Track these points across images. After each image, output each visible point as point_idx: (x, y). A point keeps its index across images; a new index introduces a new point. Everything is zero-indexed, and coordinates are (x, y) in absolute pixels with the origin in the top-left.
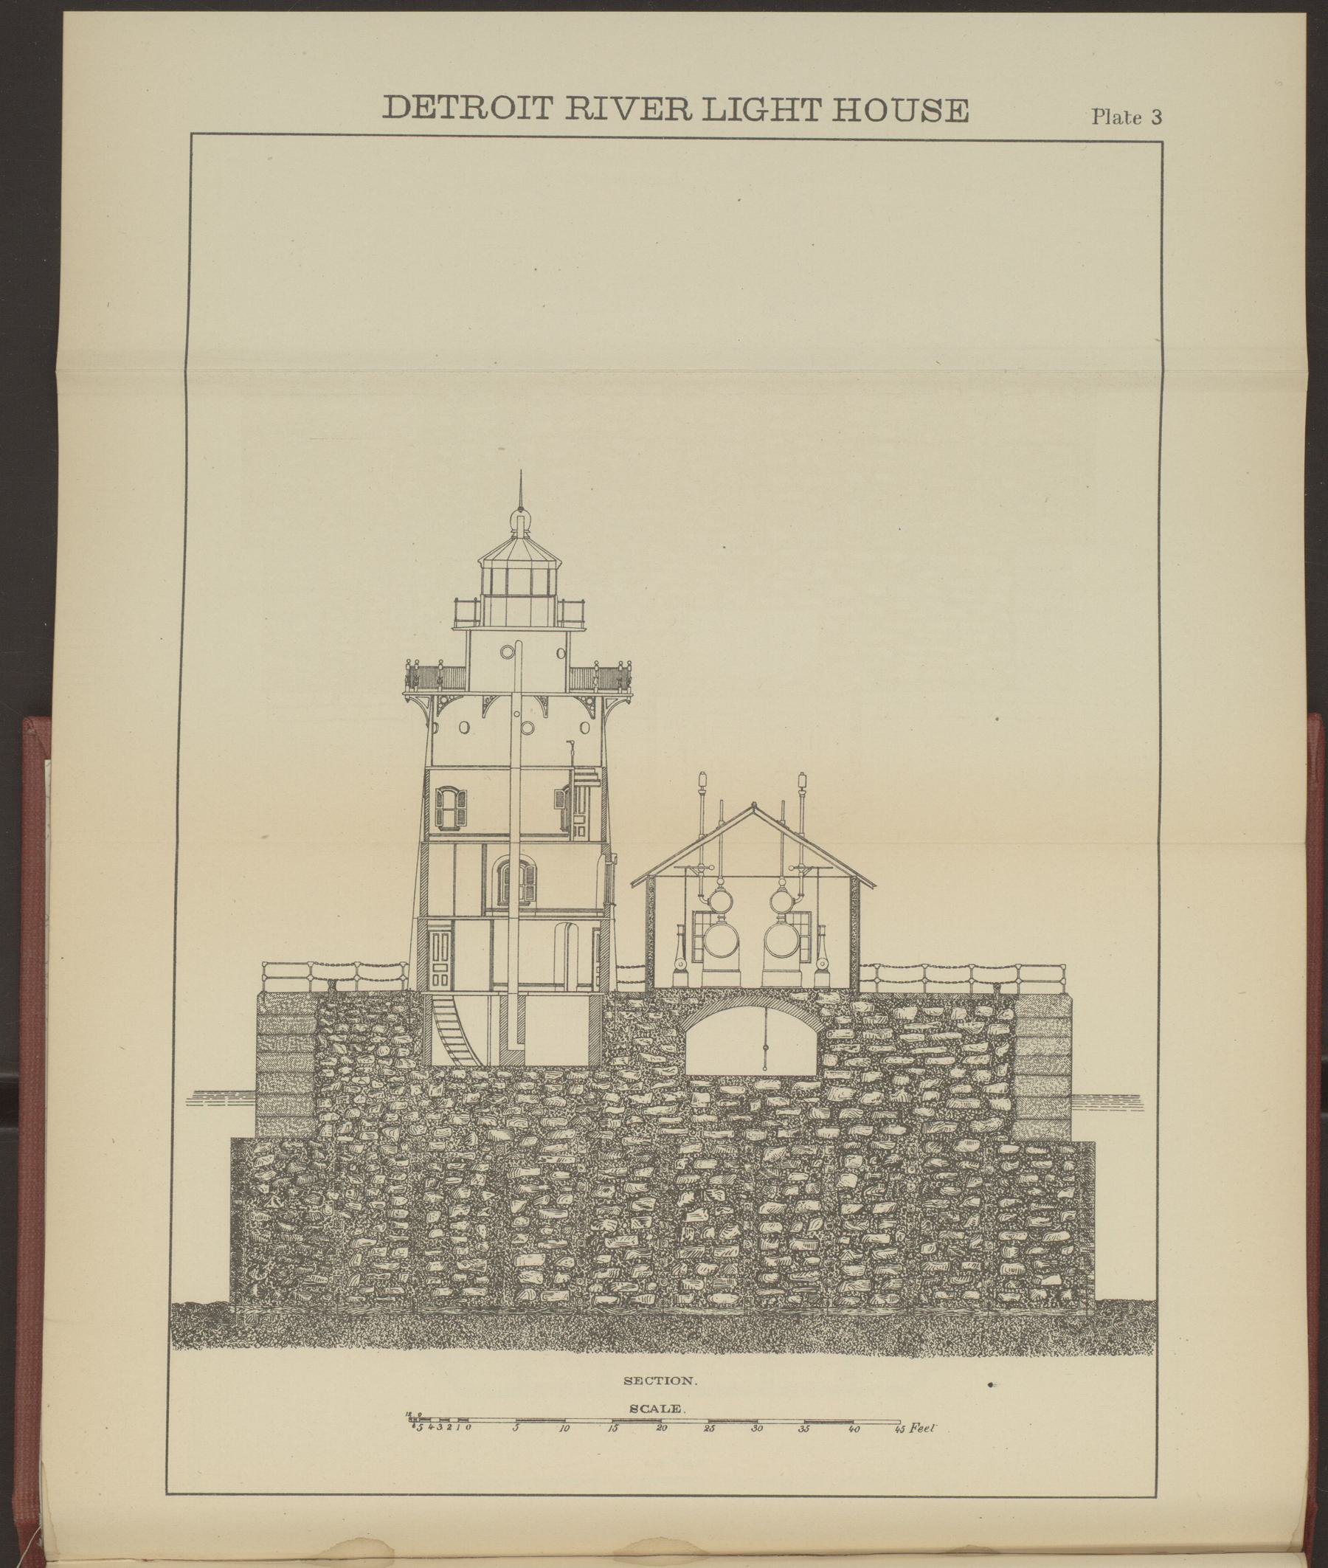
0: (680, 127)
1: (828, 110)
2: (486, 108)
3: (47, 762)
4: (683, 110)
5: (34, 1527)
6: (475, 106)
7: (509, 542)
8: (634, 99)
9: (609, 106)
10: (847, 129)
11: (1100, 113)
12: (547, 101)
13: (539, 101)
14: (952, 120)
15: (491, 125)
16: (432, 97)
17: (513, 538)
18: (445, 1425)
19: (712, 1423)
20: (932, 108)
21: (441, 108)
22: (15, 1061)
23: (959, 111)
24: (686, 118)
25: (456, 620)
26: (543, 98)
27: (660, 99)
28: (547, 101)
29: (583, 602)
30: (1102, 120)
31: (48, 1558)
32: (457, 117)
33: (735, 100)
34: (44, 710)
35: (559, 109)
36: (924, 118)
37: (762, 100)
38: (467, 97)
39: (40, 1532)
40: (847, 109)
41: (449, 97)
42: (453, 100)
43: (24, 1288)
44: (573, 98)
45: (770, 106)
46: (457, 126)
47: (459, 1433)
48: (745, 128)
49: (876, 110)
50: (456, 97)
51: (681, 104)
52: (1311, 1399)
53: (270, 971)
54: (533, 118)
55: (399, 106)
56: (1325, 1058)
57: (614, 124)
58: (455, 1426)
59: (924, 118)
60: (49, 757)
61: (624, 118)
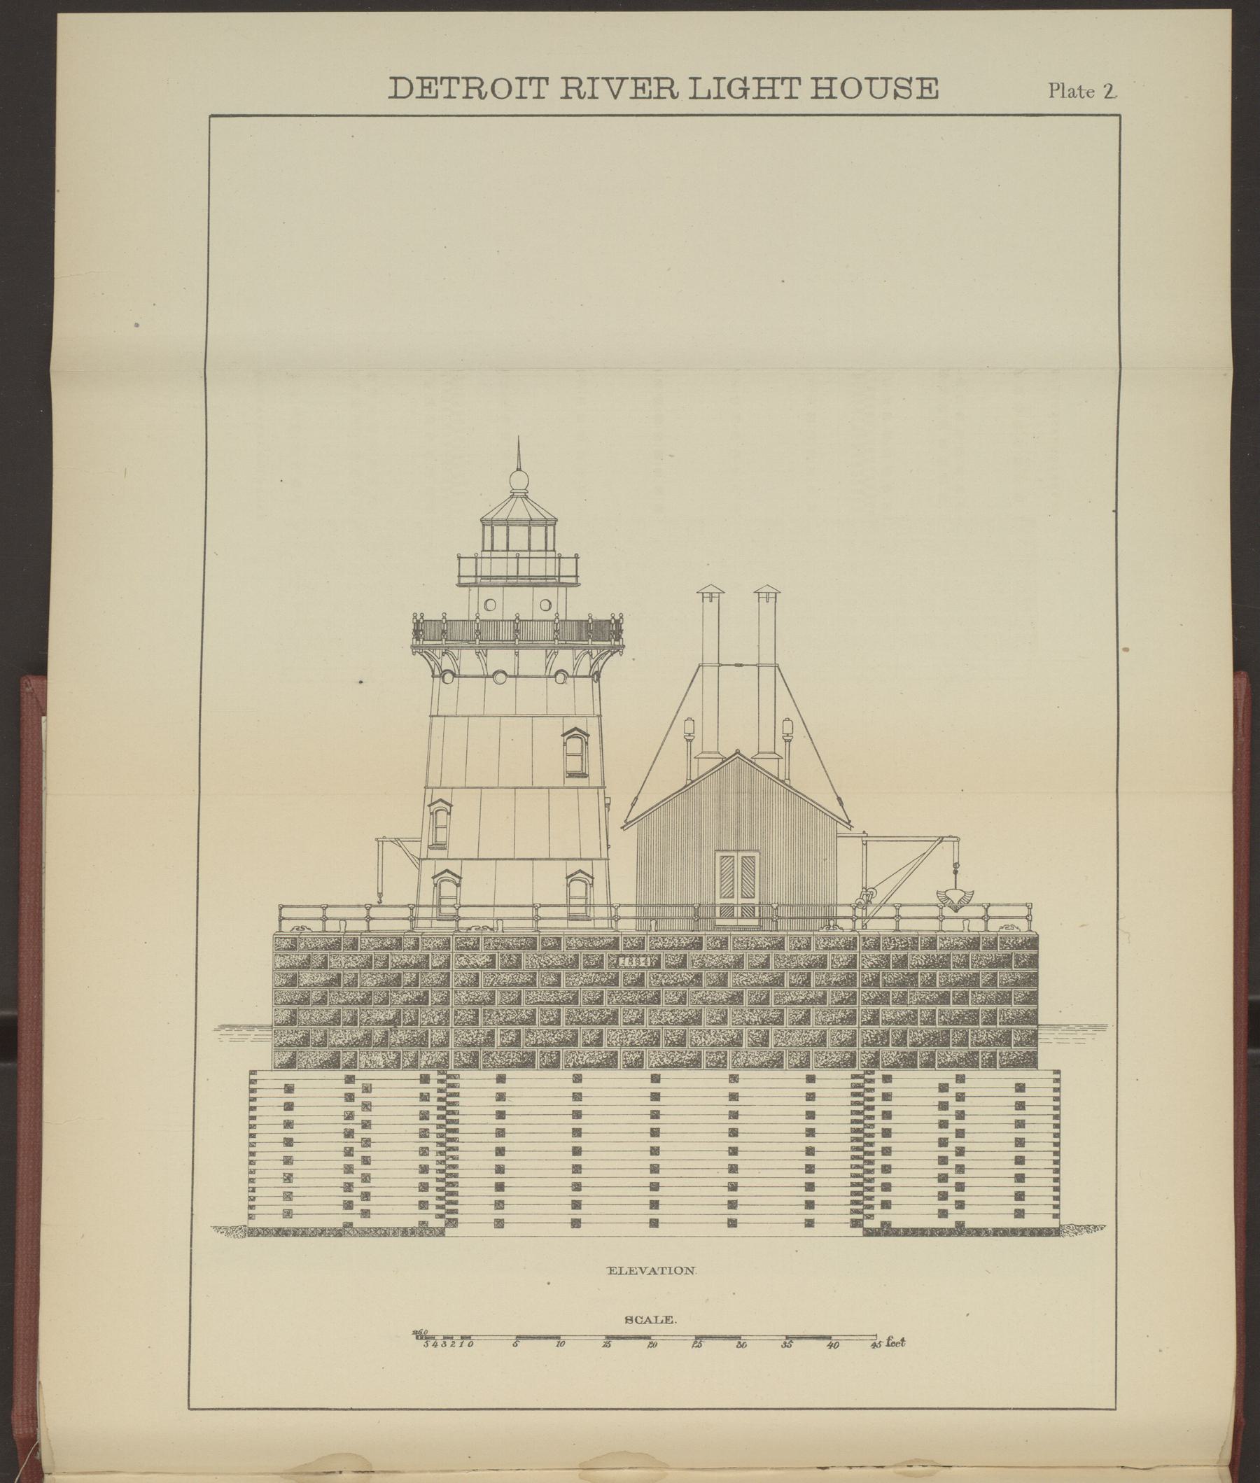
0: (667, 105)
1: (557, 87)
2: (486, 88)
3: (43, 718)
4: (670, 88)
5: (32, 1442)
6: (475, 87)
7: (506, 502)
8: (623, 79)
9: (601, 86)
10: (825, 106)
11: (1055, 87)
12: (543, 82)
13: (535, 82)
14: (922, 97)
15: (490, 105)
16: (436, 79)
17: (512, 497)
18: (449, 1342)
19: (699, 1339)
20: (900, 87)
21: (443, 89)
22: (14, 1001)
23: (928, 87)
24: (672, 96)
25: (459, 576)
26: (539, 79)
27: (649, 79)
28: (795, 82)
29: (576, 557)
30: (1058, 94)
31: (45, 1471)
32: (530, 97)
33: (719, 79)
34: (40, 668)
35: (554, 90)
36: (896, 95)
37: (745, 81)
38: (467, 79)
39: (38, 1446)
40: (825, 87)
41: (450, 78)
42: (454, 82)
43: (22, 1215)
44: (566, 79)
45: (753, 85)
46: (459, 106)
47: (459, 1353)
48: (728, 105)
49: (851, 88)
50: (458, 79)
51: (576, 83)
52: (1238, 1319)
53: (286, 913)
54: (530, 97)
55: (403, 88)
56: (1251, 998)
57: (605, 103)
58: (458, 1343)
59: (896, 95)
60: (45, 714)
61: (615, 97)
